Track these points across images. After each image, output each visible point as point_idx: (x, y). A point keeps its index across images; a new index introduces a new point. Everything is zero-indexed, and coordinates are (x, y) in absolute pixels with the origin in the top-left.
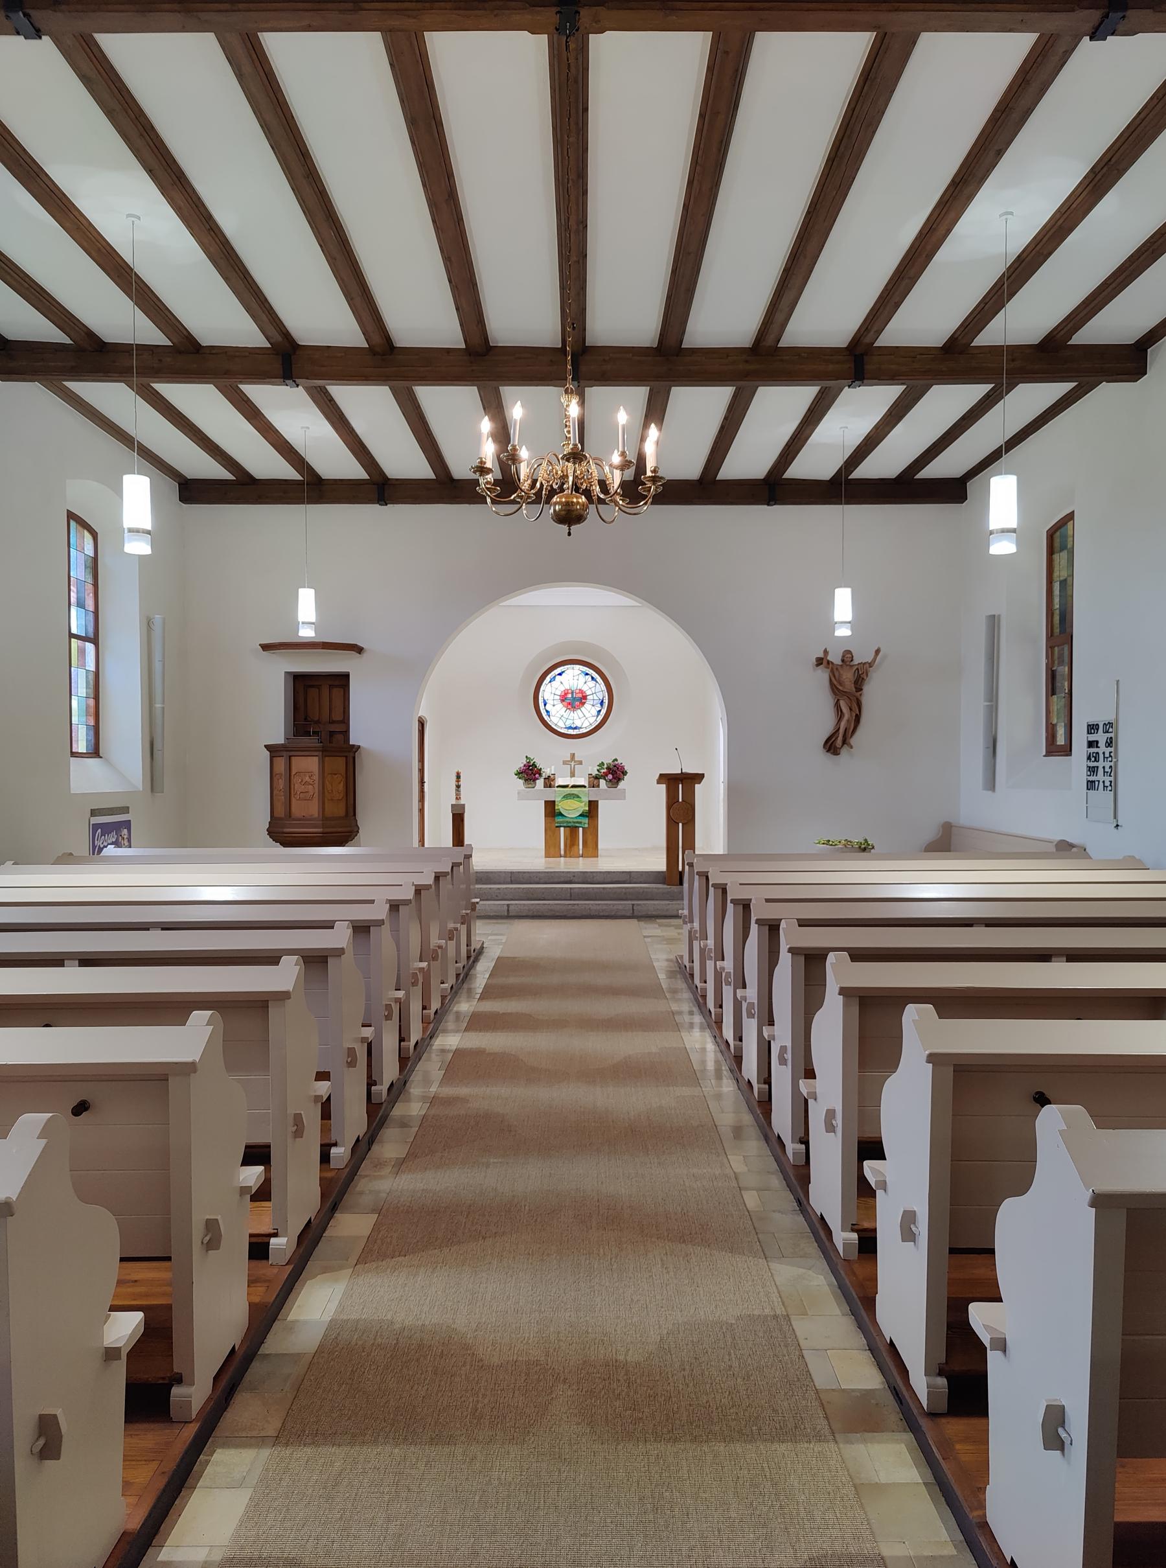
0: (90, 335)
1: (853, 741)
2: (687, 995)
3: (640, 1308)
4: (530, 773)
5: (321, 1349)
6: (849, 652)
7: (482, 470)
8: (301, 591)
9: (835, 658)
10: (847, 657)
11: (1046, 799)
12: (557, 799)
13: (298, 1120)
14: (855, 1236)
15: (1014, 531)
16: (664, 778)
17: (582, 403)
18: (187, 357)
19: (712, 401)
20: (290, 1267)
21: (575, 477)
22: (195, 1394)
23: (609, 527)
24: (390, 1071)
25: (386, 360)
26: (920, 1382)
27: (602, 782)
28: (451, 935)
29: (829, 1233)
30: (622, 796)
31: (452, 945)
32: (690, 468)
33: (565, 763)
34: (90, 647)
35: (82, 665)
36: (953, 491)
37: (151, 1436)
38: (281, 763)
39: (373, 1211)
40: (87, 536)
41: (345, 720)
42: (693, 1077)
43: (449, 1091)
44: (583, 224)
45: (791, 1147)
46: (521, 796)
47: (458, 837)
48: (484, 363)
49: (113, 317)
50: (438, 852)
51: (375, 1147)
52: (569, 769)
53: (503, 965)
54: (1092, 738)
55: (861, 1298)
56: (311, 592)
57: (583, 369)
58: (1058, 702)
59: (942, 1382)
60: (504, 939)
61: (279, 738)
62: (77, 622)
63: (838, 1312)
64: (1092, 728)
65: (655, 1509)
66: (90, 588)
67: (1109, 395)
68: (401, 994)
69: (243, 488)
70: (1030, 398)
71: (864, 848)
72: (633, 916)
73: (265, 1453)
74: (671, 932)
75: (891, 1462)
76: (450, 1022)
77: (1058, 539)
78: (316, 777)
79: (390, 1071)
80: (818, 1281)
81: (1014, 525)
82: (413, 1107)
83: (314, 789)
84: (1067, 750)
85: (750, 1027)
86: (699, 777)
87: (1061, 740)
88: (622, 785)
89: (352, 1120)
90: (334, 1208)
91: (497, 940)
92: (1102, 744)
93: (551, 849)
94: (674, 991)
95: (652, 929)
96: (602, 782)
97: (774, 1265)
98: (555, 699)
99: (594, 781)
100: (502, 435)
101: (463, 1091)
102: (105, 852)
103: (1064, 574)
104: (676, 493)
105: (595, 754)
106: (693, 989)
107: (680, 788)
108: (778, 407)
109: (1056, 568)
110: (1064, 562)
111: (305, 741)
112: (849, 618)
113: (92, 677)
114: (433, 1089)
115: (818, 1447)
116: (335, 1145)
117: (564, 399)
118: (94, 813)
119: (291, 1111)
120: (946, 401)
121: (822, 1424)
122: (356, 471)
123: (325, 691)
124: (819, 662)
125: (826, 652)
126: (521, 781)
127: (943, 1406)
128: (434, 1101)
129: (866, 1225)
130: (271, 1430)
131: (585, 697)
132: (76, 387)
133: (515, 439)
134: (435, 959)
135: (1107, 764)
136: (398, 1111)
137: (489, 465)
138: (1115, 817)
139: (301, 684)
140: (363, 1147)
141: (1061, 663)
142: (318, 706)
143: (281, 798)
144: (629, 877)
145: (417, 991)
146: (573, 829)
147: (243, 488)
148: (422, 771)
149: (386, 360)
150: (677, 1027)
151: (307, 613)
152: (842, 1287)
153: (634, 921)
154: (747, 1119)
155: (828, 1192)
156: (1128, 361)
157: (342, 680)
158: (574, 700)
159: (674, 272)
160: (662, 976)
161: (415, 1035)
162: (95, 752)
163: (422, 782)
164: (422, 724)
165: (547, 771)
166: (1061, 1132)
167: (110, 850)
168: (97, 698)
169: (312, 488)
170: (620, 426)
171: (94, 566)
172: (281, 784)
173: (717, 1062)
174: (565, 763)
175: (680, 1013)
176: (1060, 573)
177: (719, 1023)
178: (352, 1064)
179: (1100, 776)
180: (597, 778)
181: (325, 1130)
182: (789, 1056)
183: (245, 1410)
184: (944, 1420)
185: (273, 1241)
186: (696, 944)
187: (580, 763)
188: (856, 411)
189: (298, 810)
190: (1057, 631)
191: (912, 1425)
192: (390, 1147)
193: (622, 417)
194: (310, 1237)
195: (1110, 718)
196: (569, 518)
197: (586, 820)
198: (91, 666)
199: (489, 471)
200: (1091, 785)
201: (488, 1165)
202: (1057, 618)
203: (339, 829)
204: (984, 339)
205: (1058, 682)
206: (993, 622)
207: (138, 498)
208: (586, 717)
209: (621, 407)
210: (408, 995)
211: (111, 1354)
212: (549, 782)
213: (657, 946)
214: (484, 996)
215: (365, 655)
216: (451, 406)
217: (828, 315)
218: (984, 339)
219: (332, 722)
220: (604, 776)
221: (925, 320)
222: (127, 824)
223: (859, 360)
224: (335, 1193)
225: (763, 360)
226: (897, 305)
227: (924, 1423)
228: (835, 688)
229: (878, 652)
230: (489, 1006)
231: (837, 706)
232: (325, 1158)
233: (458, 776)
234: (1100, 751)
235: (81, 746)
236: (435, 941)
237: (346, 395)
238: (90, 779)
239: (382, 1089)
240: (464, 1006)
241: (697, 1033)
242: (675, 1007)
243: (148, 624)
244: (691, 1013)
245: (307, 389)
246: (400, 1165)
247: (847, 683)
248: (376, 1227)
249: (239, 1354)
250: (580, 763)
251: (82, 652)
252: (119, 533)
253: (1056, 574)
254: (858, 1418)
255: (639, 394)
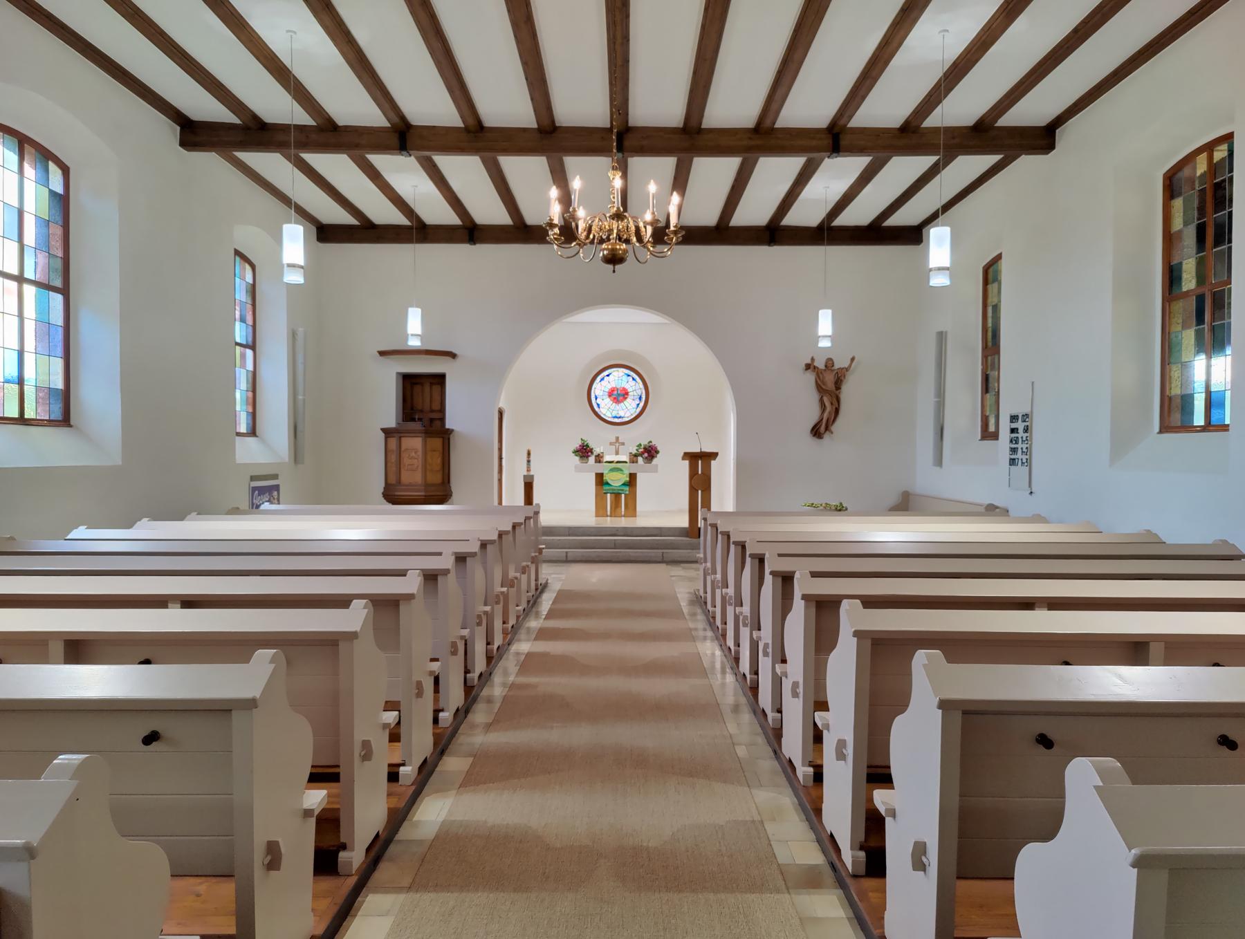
0: (255, 117)
1: (833, 428)
2: (701, 617)
3: (657, 816)
4: (584, 451)
5: (437, 837)
6: (830, 359)
7: (552, 225)
8: (410, 310)
9: (820, 364)
10: (829, 363)
11: (978, 471)
12: (605, 472)
13: (419, 685)
14: (811, 770)
15: (947, 269)
16: (687, 456)
17: (625, 176)
18: (329, 134)
19: (727, 166)
20: (413, 788)
21: (619, 230)
22: (354, 857)
23: (644, 264)
24: (480, 665)
25: (477, 137)
26: (848, 856)
27: (640, 459)
28: (524, 570)
29: (794, 768)
30: (655, 470)
31: (524, 578)
32: (708, 216)
33: (611, 444)
34: (249, 353)
35: (243, 365)
36: (913, 235)
37: (327, 883)
38: (393, 442)
39: (470, 756)
40: (248, 267)
41: (442, 410)
42: (704, 673)
43: (523, 680)
44: (626, 38)
45: (771, 715)
46: (577, 469)
47: (529, 499)
48: (551, 139)
49: (274, 105)
50: (513, 509)
51: (470, 716)
52: (615, 451)
53: (562, 596)
54: (1014, 426)
55: (813, 809)
56: (829, 312)
57: (627, 143)
58: (990, 397)
59: (862, 854)
60: (563, 577)
61: (391, 423)
62: (240, 333)
63: (797, 819)
64: (1014, 418)
65: (665, 929)
66: (249, 307)
67: (1027, 164)
68: (488, 608)
69: (366, 231)
70: (968, 166)
71: (840, 509)
72: (663, 561)
73: (402, 897)
74: (691, 573)
75: (828, 906)
76: (522, 634)
77: (990, 274)
78: (420, 453)
79: (480, 665)
80: (786, 800)
81: (948, 265)
82: (497, 689)
83: (418, 462)
84: (995, 436)
85: (745, 633)
86: (714, 455)
87: (992, 428)
88: (655, 461)
89: (454, 696)
90: (442, 753)
91: (557, 578)
92: (1021, 430)
93: (600, 510)
94: (693, 615)
95: (677, 571)
96: (640, 459)
97: (755, 791)
98: (608, 395)
99: (634, 458)
100: (566, 200)
101: (533, 680)
102: (262, 507)
103: (995, 301)
104: (694, 236)
105: (635, 438)
106: (706, 612)
107: (700, 461)
108: (774, 173)
109: (990, 295)
110: (995, 290)
111: (416, 426)
112: (830, 333)
113: (250, 375)
114: (511, 679)
115: (777, 896)
116: (442, 710)
117: (610, 174)
118: (253, 478)
119: (415, 678)
120: (903, 169)
121: (781, 883)
122: (452, 219)
123: (427, 388)
124: (808, 367)
125: (813, 359)
126: (577, 458)
127: (862, 870)
128: (513, 686)
129: (819, 762)
130: (406, 882)
131: (627, 393)
132: (243, 156)
133: (575, 202)
134: (512, 586)
135: (1025, 446)
136: (485, 692)
137: (556, 221)
138: (1030, 485)
139: (410, 382)
140: (462, 713)
141: (993, 368)
142: (421, 399)
143: (393, 469)
144: (660, 531)
145: (499, 609)
146: (617, 496)
147: (366, 231)
148: (500, 449)
149: (477, 137)
150: (694, 639)
151: (414, 327)
152: (801, 804)
153: (663, 566)
154: (743, 700)
155: (794, 744)
156: (1042, 139)
157: (440, 379)
158: (619, 396)
159: (695, 73)
160: (684, 604)
161: (498, 641)
162: (253, 432)
163: (500, 458)
164: (501, 413)
165: (597, 450)
166: (924, 666)
167: (266, 506)
168: (254, 391)
169: (419, 231)
170: (653, 189)
171: (253, 290)
172: (393, 458)
173: (722, 663)
174: (611, 444)
175: (696, 629)
176: (992, 300)
177: (724, 636)
178: (454, 653)
179: (1019, 455)
180: (636, 456)
181: (436, 700)
182: (770, 650)
183: (384, 872)
184: (863, 880)
185: (402, 769)
186: (709, 578)
187: (623, 444)
188: (834, 176)
189: (406, 477)
190: (990, 344)
191: (841, 884)
192: (479, 715)
193: (652, 188)
194: (427, 770)
195: (1027, 410)
196: (614, 259)
197: (627, 488)
198: (250, 367)
199: (556, 226)
200: (1013, 462)
201: (552, 728)
202: (990, 334)
203: (439, 493)
204: (931, 122)
205: (988, 384)
206: (941, 337)
207: (294, 243)
208: (628, 409)
209: (652, 175)
210: (493, 609)
211: (307, 813)
212: (599, 459)
213: (680, 584)
214: (548, 617)
215: (458, 360)
216: (525, 171)
217: (811, 105)
218: (931, 122)
219: (432, 411)
220: (641, 455)
221: (886, 107)
222: (277, 488)
223: (835, 138)
224: (443, 744)
225: (763, 138)
226: (864, 98)
227: (849, 881)
228: (820, 388)
229: (853, 359)
230: (552, 624)
231: (821, 401)
232: (436, 721)
233: (529, 454)
234: (1019, 435)
235: (243, 428)
236: (512, 574)
237: (448, 163)
238: (250, 453)
239: (474, 676)
240: (534, 624)
241: (708, 644)
242: (691, 625)
243: (293, 335)
244: (705, 630)
245: (417, 158)
246: (488, 727)
247: (830, 383)
248: (473, 765)
249: (382, 837)
250: (623, 444)
251: (243, 356)
252: (279, 267)
253: (990, 300)
254: (809, 880)
255: (667, 164)
